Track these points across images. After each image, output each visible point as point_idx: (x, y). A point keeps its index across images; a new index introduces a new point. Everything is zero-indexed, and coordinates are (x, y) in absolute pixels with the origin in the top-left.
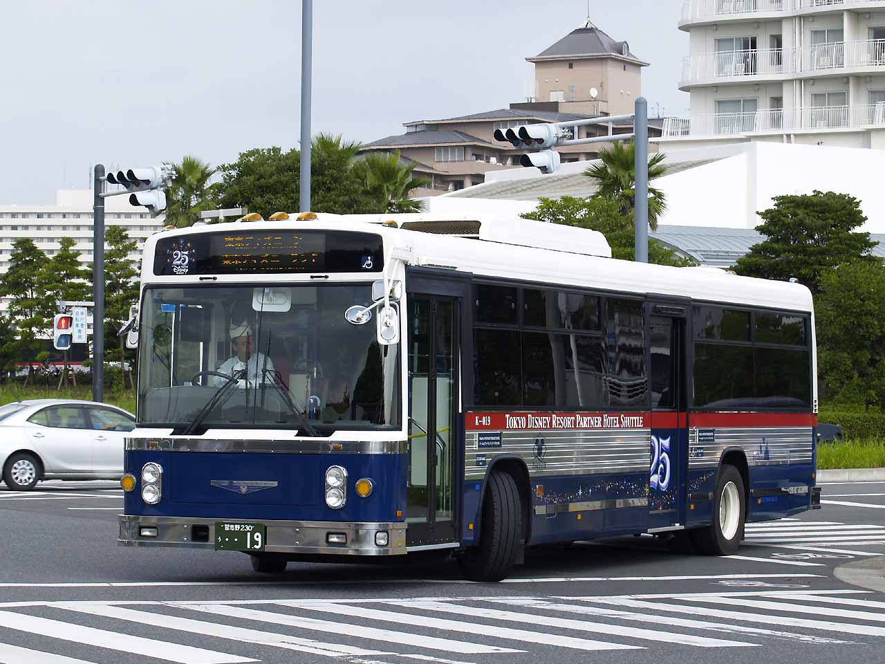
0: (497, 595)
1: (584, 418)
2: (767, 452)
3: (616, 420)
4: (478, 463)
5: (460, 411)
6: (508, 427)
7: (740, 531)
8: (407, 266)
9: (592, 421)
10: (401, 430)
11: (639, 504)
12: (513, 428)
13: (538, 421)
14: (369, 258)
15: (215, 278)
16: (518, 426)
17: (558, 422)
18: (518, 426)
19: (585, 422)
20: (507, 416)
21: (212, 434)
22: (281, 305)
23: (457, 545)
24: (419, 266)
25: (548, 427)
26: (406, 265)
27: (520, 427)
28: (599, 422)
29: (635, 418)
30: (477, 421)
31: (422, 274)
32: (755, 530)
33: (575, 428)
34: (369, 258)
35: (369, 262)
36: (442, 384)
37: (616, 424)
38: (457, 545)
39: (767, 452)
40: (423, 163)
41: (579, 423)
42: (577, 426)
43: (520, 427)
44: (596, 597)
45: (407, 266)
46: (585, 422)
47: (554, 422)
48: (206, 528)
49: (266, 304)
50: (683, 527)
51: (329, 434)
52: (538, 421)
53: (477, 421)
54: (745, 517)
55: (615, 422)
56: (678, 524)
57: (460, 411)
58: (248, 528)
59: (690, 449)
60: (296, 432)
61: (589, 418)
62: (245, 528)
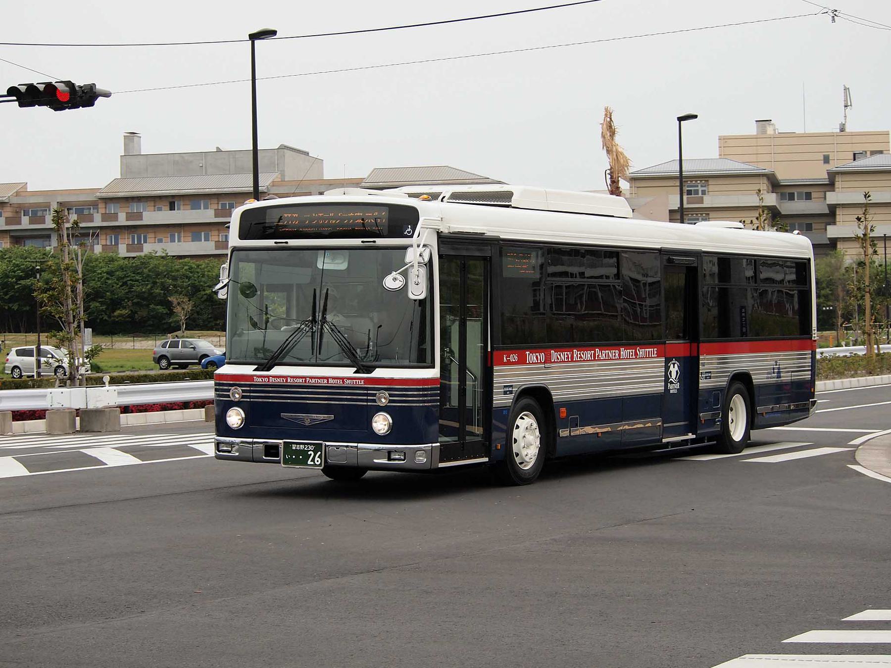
0: (697, 458)
1: (603, 351)
2: (779, 373)
3: (632, 352)
4: (505, 393)
5: (489, 350)
6: (528, 362)
7: (747, 435)
8: (439, 235)
9: (610, 353)
10: (434, 368)
11: (493, 446)
12: (533, 363)
13: (560, 356)
14: (410, 226)
15: (287, 243)
16: (538, 361)
17: (579, 356)
18: (538, 361)
19: (604, 355)
20: (528, 353)
21: (277, 371)
22: (338, 264)
23: (486, 460)
24: (450, 233)
25: (570, 360)
26: (438, 232)
27: (539, 361)
28: (617, 355)
29: (650, 349)
30: (505, 358)
31: (450, 238)
32: (755, 435)
33: (595, 360)
34: (410, 226)
35: (409, 229)
36: (474, 328)
37: (632, 355)
38: (486, 460)
39: (779, 373)
40: (673, 218)
41: (598, 356)
42: (597, 359)
43: (539, 361)
44: (752, 459)
45: (439, 235)
46: (604, 355)
47: (575, 355)
48: (276, 447)
49: (326, 263)
50: (694, 436)
51: (269, 370)
52: (560, 356)
53: (505, 358)
54: (751, 424)
55: (631, 354)
56: (691, 434)
57: (489, 350)
58: (310, 448)
59: (700, 373)
60: (355, 369)
61: (607, 351)
62: (308, 448)
